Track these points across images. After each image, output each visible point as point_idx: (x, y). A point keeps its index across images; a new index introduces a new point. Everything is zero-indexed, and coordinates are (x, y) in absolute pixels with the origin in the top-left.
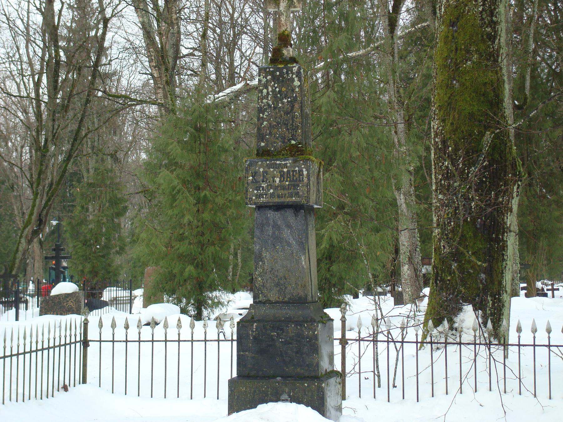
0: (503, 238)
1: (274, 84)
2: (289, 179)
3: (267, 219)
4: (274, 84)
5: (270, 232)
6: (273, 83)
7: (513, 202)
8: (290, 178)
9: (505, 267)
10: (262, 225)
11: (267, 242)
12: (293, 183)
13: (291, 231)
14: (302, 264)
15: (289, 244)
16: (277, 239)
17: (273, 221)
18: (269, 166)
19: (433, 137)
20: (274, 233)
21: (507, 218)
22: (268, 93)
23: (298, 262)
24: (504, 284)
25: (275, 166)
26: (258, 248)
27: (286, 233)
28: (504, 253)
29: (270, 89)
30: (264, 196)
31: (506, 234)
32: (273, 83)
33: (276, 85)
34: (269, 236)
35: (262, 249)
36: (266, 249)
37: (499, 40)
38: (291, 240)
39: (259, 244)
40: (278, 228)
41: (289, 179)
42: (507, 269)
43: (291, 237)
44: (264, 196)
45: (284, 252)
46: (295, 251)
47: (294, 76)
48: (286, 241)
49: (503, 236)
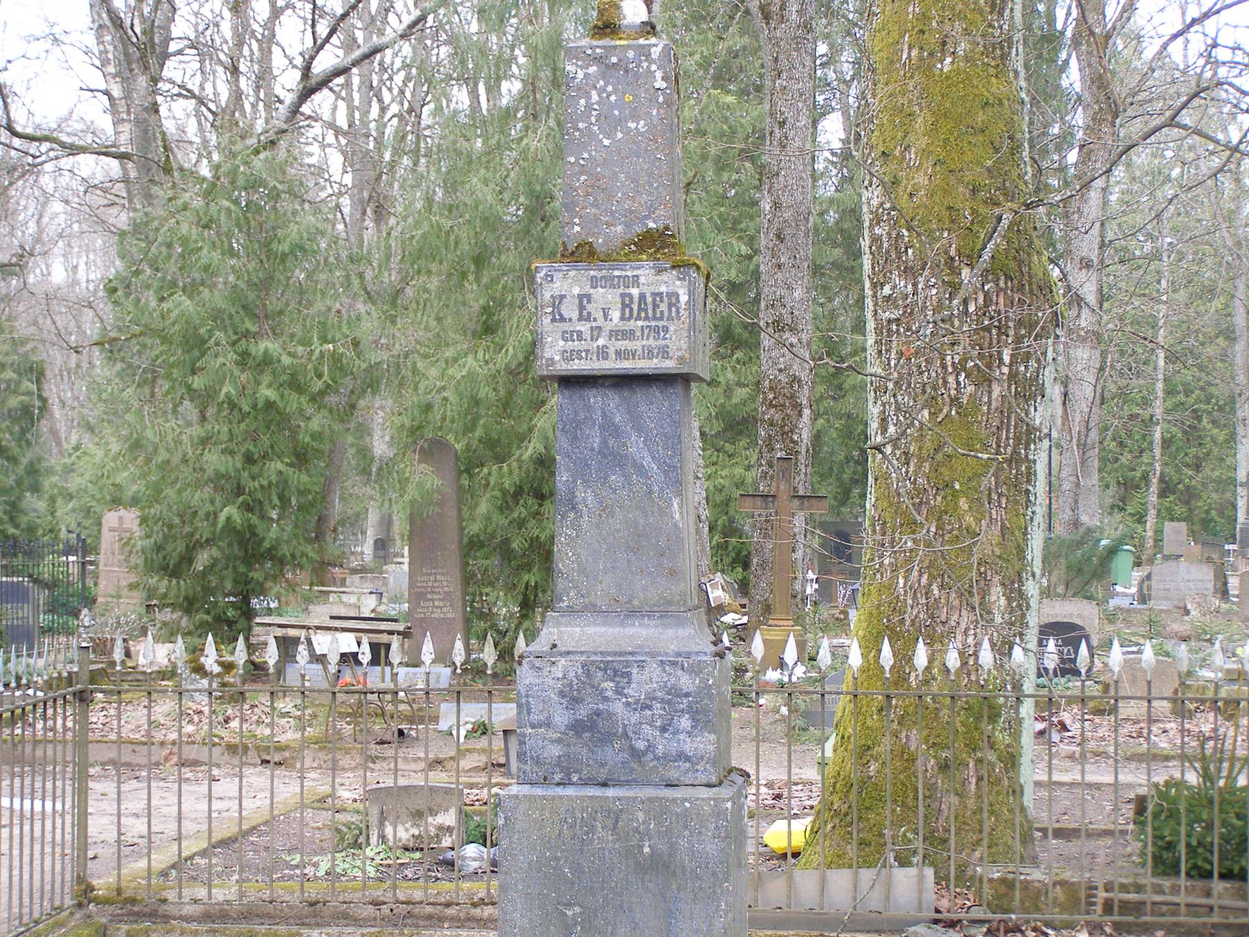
0: (1026, 456)
1: (606, 85)
2: (643, 315)
3: (589, 408)
4: (606, 85)
5: (596, 442)
6: (602, 83)
7: (1046, 373)
8: (646, 311)
9: (1032, 519)
10: (577, 425)
11: (587, 465)
12: (653, 323)
13: (646, 439)
14: (673, 518)
15: (640, 470)
16: (614, 458)
17: (604, 413)
18: (594, 283)
19: (867, 224)
20: (604, 442)
21: (1036, 410)
22: (589, 107)
23: (665, 512)
24: (1029, 558)
25: (609, 282)
26: (564, 479)
27: (635, 446)
28: (1030, 488)
29: (595, 97)
30: (583, 354)
31: (1032, 447)
32: (602, 83)
33: (610, 88)
34: (592, 450)
35: (575, 481)
36: (584, 481)
37: (1012, 10)
38: (647, 461)
39: (568, 470)
40: (616, 431)
41: (643, 315)
42: (1035, 523)
43: (646, 454)
44: (583, 354)
45: (630, 490)
46: (656, 488)
47: (654, 67)
48: (635, 463)
49: (1027, 448)
